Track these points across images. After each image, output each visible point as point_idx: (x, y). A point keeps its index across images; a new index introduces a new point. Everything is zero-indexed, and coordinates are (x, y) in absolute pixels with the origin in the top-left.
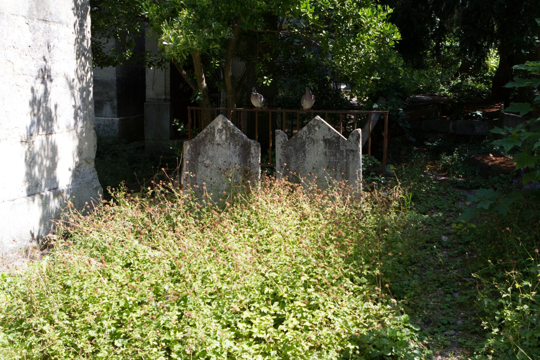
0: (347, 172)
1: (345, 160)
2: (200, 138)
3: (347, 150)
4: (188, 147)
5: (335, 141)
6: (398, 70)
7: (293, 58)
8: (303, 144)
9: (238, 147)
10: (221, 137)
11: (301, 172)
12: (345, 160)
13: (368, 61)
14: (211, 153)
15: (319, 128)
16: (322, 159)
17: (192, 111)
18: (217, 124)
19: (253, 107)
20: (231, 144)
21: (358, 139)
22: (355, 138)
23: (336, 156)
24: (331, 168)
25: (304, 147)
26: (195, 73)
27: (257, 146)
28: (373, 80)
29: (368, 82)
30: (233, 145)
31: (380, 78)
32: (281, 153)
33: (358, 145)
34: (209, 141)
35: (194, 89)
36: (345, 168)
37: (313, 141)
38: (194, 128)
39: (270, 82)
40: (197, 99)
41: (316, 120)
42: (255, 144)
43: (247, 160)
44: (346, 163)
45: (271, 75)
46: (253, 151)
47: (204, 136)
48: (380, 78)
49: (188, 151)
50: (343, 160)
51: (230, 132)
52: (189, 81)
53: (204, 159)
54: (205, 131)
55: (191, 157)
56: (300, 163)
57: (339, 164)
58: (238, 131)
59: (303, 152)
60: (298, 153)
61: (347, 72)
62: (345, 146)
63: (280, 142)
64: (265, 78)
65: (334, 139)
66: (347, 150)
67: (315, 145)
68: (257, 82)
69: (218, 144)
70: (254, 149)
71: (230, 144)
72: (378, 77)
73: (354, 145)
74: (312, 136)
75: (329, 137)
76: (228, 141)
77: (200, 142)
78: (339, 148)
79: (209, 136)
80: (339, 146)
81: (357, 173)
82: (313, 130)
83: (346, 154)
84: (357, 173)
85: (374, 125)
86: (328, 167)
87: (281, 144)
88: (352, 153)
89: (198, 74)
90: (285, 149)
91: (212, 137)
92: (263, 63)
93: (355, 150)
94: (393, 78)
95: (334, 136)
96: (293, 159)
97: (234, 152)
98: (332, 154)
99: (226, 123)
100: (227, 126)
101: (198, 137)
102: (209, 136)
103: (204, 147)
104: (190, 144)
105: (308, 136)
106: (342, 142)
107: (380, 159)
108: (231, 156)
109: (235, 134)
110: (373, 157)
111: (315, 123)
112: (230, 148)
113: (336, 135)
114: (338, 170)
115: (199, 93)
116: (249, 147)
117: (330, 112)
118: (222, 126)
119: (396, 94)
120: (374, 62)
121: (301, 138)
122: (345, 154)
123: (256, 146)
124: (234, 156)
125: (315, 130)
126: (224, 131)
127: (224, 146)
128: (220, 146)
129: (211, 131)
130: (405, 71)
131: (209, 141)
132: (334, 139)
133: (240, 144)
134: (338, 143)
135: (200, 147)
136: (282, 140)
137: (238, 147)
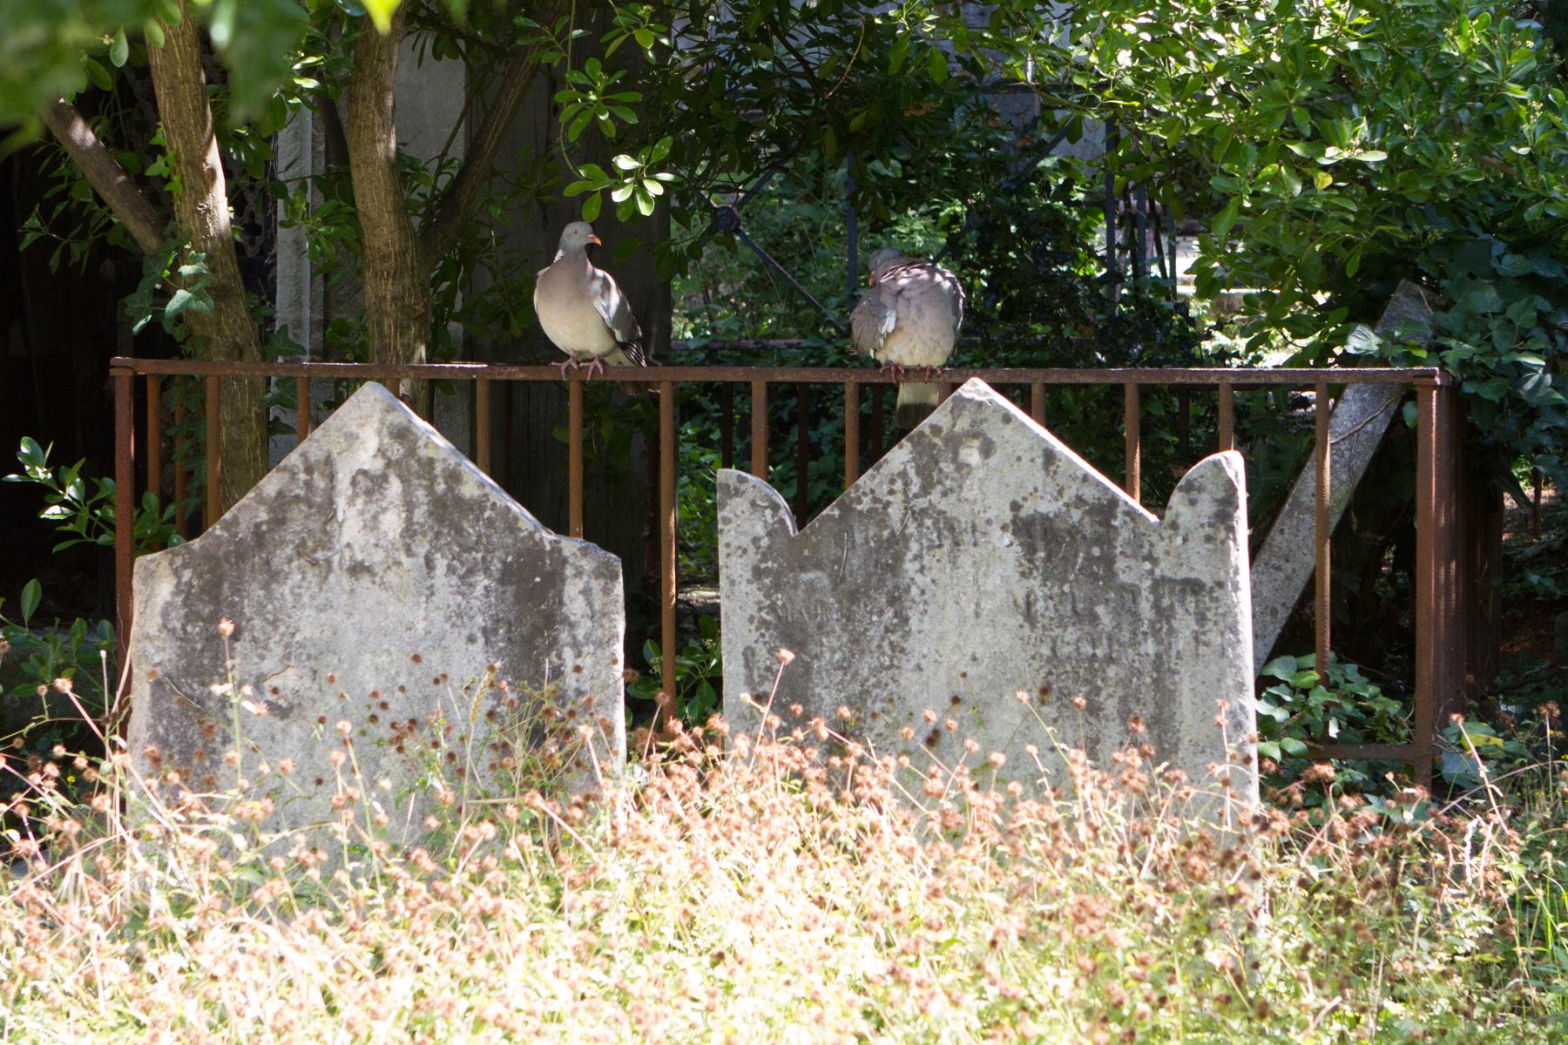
0: (1162, 723)
1: (1150, 647)
2: (244, 531)
3: (1158, 584)
4: (165, 589)
5: (1088, 530)
6: (1505, 102)
7: (801, 35)
8: (890, 553)
9: (482, 581)
10: (373, 524)
11: (879, 726)
12: (1150, 647)
13: (1301, 51)
14: (308, 626)
15: (987, 450)
16: (1006, 641)
17: (139, 384)
18: (351, 438)
19: (545, 351)
20: (441, 564)
21: (1224, 516)
22: (1207, 507)
23: (1094, 618)
24: (1066, 695)
25: (895, 568)
26: (160, 138)
27: (605, 573)
28: (1337, 169)
29: (1309, 183)
30: (451, 570)
31: (1381, 156)
32: (752, 610)
33: (1225, 553)
34: (301, 550)
35: (144, 235)
36: (1148, 696)
37: (950, 531)
38: (151, 498)
39: (655, 189)
40: (173, 305)
41: (962, 403)
42: (587, 564)
43: (538, 665)
44: (1158, 662)
45: (664, 148)
46: (575, 605)
47: (263, 516)
48: (1381, 156)
49: (165, 614)
50: (1134, 643)
51: (430, 489)
52: (113, 185)
53: (268, 665)
54: (271, 484)
55: (184, 654)
56: (874, 672)
57: (1112, 671)
58: (482, 485)
59: (892, 601)
60: (859, 610)
61: (1170, 123)
62: (1150, 558)
63: (745, 541)
64: (624, 162)
65: (1076, 515)
66: (1158, 584)
67: (965, 560)
68: (572, 190)
69: (357, 569)
70: (586, 592)
71: (429, 563)
72: (1365, 146)
73: (1197, 547)
74: (943, 505)
75: (1047, 507)
76: (422, 548)
77: (241, 557)
78: (1111, 573)
79: (297, 515)
80: (1108, 561)
81: (1222, 718)
82: (948, 467)
83: (1156, 606)
84: (1222, 718)
85: (1360, 464)
86: (1045, 691)
87: (753, 557)
88: (1190, 600)
89: (178, 144)
90: (777, 587)
91: (315, 524)
92: (609, 70)
93: (1208, 581)
94: (1478, 152)
95: (1080, 501)
96: (831, 648)
97: (458, 616)
98: (1067, 609)
99: (402, 434)
100: (412, 452)
101: (227, 526)
102: (298, 518)
103: (266, 586)
104: (177, 573)
105: (921, 503)
106: (1125, 534)
107: (1399, 684)
108: (439, 642)
109: (459, 501)
110: (1351, 669)
111: (963, 424)
112: (432, 592)
113: (1089, 494)
114: (1111, 706)
115: (186, 270)
116: (554, 579)
117: (1058, 376)
118: (381, 452)
119: (1512, 264)
120: (1346, 54)
121: (878, 514)
122: (1145, 607)
123: (598, 574)
124: (456, 641)
125: (961, 467)
126: (395, 487)
127: (392, 577)
128: (365, 580)
129: (309, 485)
130: (1548, 106)
131: (301, 550)
132: (1076, 515)
133: (496, 566)
134: (1106, 538)
135: (237, 590)
136: (760, 530)
137: (482, 581)
